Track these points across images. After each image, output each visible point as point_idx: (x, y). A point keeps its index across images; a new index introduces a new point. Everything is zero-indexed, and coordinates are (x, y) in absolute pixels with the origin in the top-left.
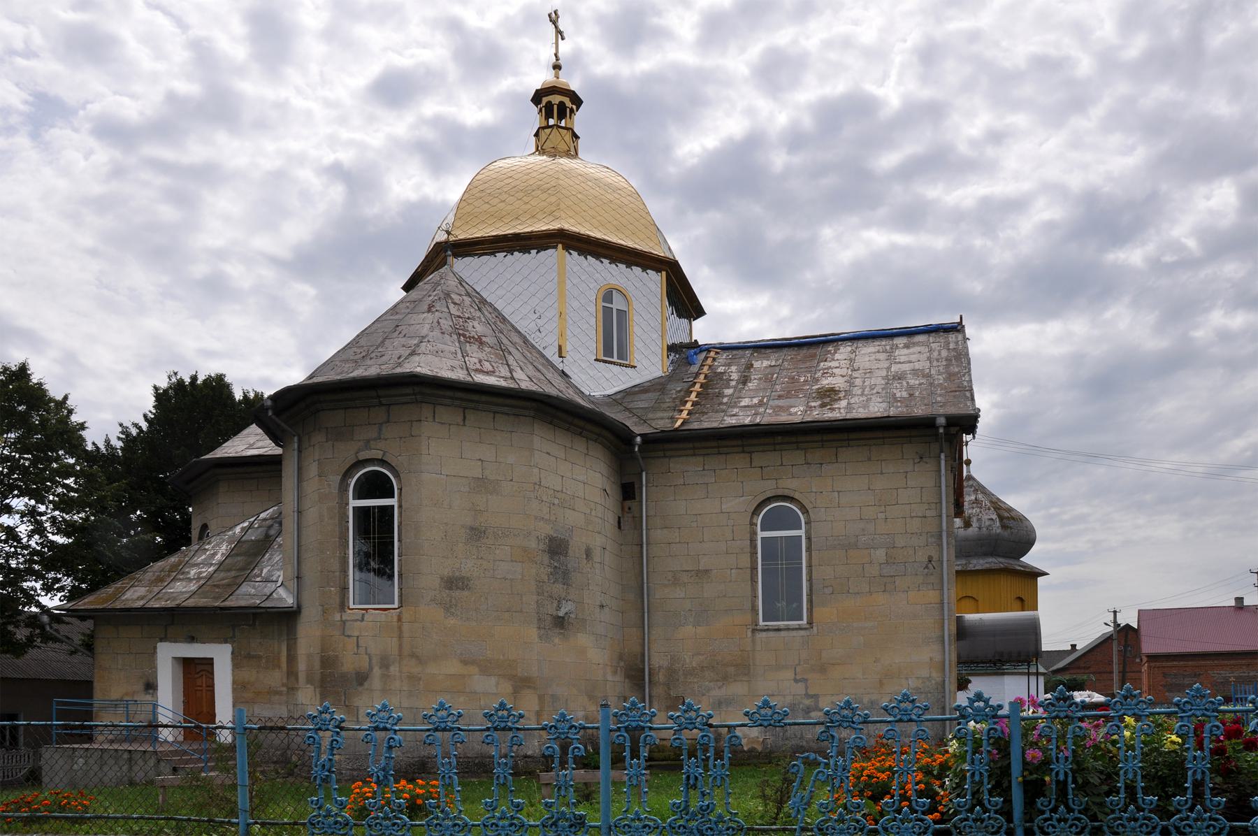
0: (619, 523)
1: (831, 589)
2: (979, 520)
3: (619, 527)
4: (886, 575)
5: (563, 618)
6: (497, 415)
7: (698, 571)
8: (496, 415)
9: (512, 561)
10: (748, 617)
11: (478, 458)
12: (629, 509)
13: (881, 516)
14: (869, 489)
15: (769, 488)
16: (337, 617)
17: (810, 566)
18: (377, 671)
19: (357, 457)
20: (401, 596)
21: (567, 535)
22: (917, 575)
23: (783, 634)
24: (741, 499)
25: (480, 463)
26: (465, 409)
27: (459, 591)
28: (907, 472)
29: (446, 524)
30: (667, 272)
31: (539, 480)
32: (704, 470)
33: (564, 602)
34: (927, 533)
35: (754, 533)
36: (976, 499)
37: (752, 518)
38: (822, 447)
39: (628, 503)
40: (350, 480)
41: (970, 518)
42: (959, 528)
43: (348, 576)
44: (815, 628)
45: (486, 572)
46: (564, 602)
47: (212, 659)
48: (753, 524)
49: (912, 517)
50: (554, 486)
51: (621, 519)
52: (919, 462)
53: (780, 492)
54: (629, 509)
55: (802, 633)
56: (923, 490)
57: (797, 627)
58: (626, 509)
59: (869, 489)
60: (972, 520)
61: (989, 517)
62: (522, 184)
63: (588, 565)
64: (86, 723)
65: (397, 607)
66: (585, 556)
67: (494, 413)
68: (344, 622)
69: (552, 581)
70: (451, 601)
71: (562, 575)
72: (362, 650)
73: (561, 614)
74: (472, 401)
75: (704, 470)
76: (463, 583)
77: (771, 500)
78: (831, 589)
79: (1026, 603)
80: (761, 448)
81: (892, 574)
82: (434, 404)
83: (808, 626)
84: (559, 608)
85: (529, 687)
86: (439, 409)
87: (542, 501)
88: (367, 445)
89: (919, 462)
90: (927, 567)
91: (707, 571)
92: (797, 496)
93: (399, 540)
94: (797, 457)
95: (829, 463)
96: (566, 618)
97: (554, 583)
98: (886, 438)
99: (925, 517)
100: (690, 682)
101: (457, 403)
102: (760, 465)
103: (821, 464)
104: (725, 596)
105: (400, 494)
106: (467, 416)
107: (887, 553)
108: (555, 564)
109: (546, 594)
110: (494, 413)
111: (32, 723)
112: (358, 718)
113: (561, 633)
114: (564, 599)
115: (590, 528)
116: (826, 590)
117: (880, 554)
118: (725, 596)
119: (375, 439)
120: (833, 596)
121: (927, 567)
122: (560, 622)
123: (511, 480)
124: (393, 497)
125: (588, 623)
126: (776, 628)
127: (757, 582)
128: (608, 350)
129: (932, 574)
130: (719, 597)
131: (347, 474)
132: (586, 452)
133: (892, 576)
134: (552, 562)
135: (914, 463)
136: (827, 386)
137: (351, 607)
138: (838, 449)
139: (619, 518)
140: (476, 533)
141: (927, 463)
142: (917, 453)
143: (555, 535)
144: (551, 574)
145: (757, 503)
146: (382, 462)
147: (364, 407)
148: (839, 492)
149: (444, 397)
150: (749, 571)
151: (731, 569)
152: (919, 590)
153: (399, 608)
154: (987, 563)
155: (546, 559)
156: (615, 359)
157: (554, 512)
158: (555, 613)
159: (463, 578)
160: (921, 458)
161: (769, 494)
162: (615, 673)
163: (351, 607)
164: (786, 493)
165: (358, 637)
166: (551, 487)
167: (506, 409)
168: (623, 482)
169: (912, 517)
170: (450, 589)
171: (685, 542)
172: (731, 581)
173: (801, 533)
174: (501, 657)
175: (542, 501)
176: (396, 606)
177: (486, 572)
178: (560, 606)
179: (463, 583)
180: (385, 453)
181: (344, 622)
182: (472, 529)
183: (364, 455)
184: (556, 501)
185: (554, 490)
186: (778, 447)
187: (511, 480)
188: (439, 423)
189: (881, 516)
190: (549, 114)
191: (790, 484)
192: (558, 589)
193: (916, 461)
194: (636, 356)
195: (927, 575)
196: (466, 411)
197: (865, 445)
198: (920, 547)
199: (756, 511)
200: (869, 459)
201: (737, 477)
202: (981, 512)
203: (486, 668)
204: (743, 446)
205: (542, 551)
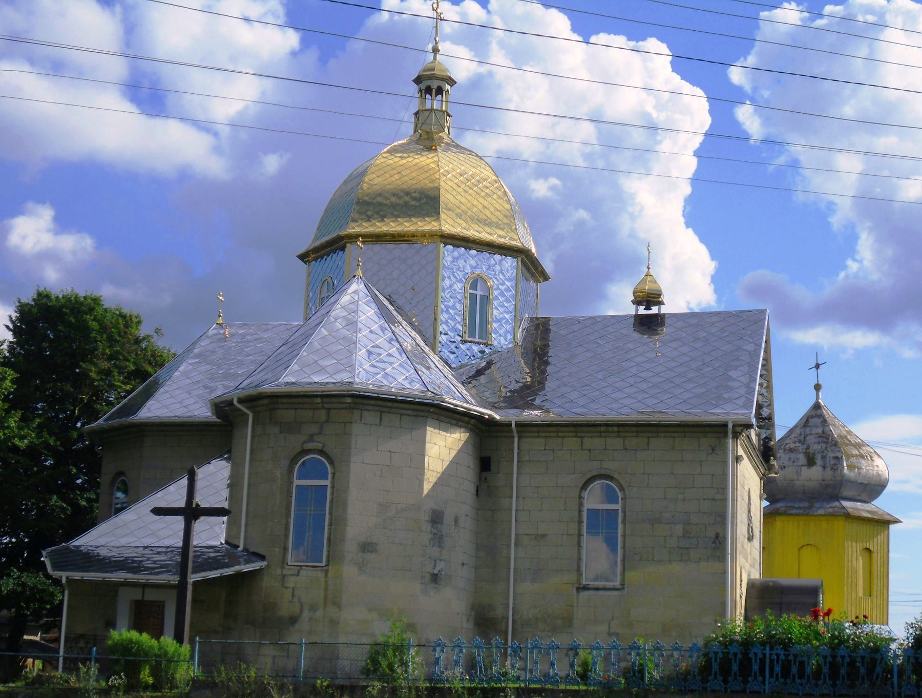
0: (477, 491)
2: (824, 457)
3: (477, 495)
4: (682, 547)
6: (403, 417)
9: (407, 530)
11: (388, 450)
14: (672, 473)
15: (594, 468)
16: (279, 571)
17: (624, 536)
18: (306, 614)
19: (303, 447)
20: (328, 556)
22: (706, 548)
23: (601, 593)
24: (575, 475)
26: (382, 412)
27: (369, 554)
32: (545, 449)
33: (438, 561)
36: (823, 432)
37: (580, 492)
39: (484, 474)
40: (295, 466)
41: (814, 454)
42: (802, 465)
43: (288, 539)
44: (626, 589)
47: (164, 602)
49: (704, 499)
50: (437, 469)
51: (479, 487)
52: (711, 454)
53: (603, 472)
54: (486, 479)
55: (616, 593)
57: (612, 587)
58: (483, 479)
59: (672, 473)
60: (816, 457)
61: (836, 455)
62: (410, 181)
64: (234, 641)
65: (324, 565)
66: (454, 524)
67: (401, 414)
68: (284, 576)
70: (363, 562)
71: (438, 539)
72: (296, 599)
73: (436, 572)
74: (386, 407)
75: (545, 449)
76: (372, 547)
77: (596, 477)
79: (874, 555)
80: (590, 435)
81: (687, 546)
82: (361, 409)
83: (620, 587)
86: (365, 413)
88: (311, 439)
89: (711, 454)
90: (714, 542)
92: (616, 476)
93: (330, 513)
95: (642, 450)
96: (439, 575)
97: (433, 547)
98: (687, 432)
100: (527, 631)
101: (377, 408)
102: (588, 448)
104: (557, 558)
105: (333, 477)
106: (383, 418)
107: (684, 528)
108: (435, 531)
110: (401, 414)
111: (228, 641)
112: (288, 653)
113: (435, 587)
116: (636, 556)
117: (679, 529)
118: (557, 558)
119: (318, 434)
121: (714, 542)
122: (435, 578)
124: (328, 480)
126: (596, 587)
131: (294, 461)
133: (687, 548)
135: (708, 454)
137: (289, 564)
138: (651, 439)
139: (478, 486)
141: (717, 454)
145: (584, 481)
146: (321, 452)
147: (310, 409)
148: (649, 474)
149: (367, 405)
150: (576, 537)
151: (563, 535)
153: (325, 566)
154: (831, 507)
158: (432, 572)
160: (713, 450)
161: (595, 473)
162: (468, 620)
163: (289, 564)
164: (608, 472)
165: (293, 588)
166: (435, 470)
167: (409, 412)
168: (482, 456)
169: (704, 499)
171: (528, 510)
173: (618, 507)
175: (429, 482)
176: (323, 564)
179: (372, 547)
180: (324, 445)
181: (284, 576)
183: (310, 446)
186: (603, 434)
188: (364, 424)
189: (680, 496)
192: (435, 551)
193: (710, 452)
196: (383, 414)
197: (671, 437)
198: (709, 524)
200: (673, 448)
201: (571, 458)
202: (826, 448)
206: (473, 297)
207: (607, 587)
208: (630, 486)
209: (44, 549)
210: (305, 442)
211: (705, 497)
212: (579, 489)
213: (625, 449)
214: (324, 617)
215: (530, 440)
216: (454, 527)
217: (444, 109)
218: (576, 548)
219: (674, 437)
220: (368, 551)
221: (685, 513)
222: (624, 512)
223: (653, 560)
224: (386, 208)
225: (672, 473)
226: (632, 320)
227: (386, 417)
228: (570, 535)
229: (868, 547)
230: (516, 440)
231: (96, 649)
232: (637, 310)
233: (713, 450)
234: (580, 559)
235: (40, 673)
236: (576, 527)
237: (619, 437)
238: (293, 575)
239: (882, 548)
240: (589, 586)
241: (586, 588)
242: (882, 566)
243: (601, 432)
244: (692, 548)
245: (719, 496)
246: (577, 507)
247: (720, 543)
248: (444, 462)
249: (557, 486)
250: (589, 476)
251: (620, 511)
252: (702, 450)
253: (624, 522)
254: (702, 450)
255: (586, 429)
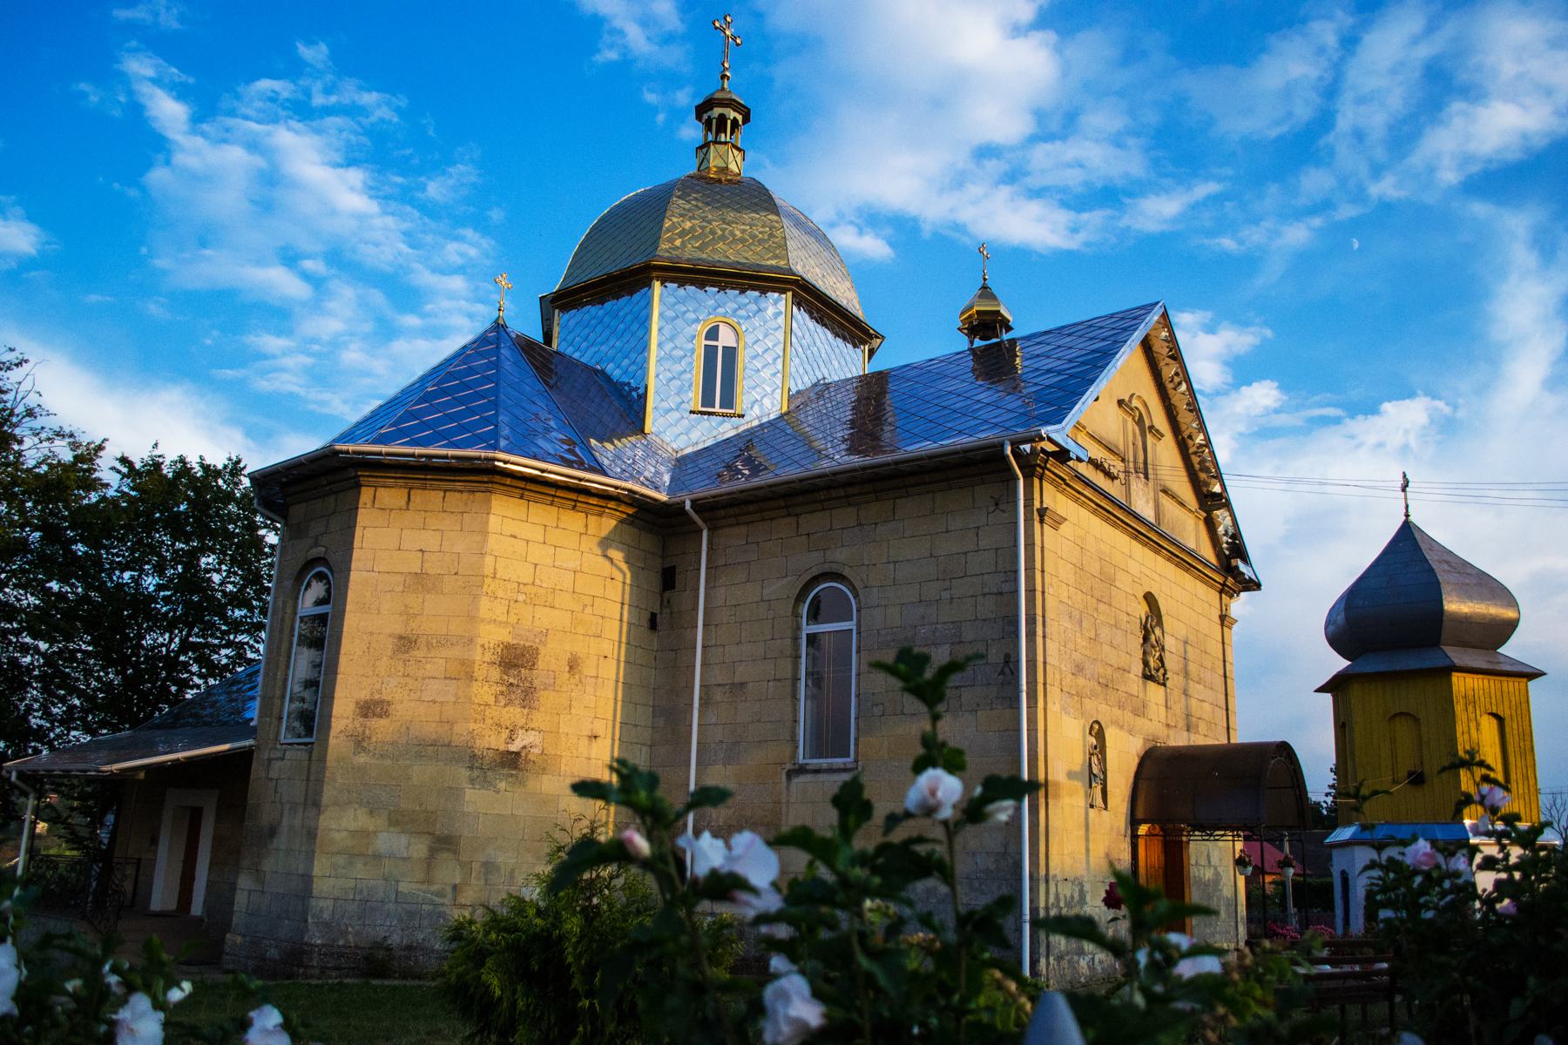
1: (881, 708)
3: (653, 624)
5: (518, 754)
7: (733, 684)
8: (448, 493)
9: (446, 678)
10: (788, 750)
12: (668, 601)
13: (946, 595)
15: (812, 562)
21: (537, 641)
24: (787, 579)
25: (420, 554)
27: (375, 719)
28: (978, 527)
29: (371, 634)
30: (793, 291)
31: (492, 571)
34: (1004, 618)
35: (798, 628)
38: (877, 500)
39: (667, 594)
45: (412, 694)
46: (520, 731)
47: (202, 808)
48: (797, 615)
49: (984, 595)
53: (827, 568)
54: (668, 601)
56: (999, 552)
57: (842, 766)
59: (931, 555)
63: (572, 680)
66: (567, 668)
69: (502, 704)
70: (364, 732)
73: (514, 748)
78: (881, 708)
84: (511, 739)
85: (449, 850)
86: (381, 492)
87: (496, 598)
91: (742, 684)
92: (847, 572)
94: (846, 516)
97: (506, 705)
99: (1001, 594)
103: (876, 524)
108: (511, 680)
109: (489, 722)
113: (512, 775)
114: (522, 728)
115: (581, 630)
120: (883, 719)
121: (1002, 673)
123: (456, 574)
125: (563, 760)
127: (799, 700)
128: (708, 399)
129: (1010, 683)
130: (753, 722)
132: (583, 530)
134: (506, 677)
136: (312, 407)
138: (897, 501)
140: (406, 643)
141: (1004, 511)
142: (992, 497)
143: (515, 642)
144: (502, 693)
148: (895, 562)
150: (788, 683)
152: (992, 709)
155: (495, 673)
156: (717, 409)
157: (516, 611)
159: (383, 702)
160: (997, 504)
161: (815, 571)
164: (835, 568)
166: (514, 578)
168: (666, 566)
169: (984, 595)
170: (366, 716)
172: (767, 699)
174: (418, 808)
177: (412, 694)
178: (514, 737)
182: (401, 638)
184: (521, 598)
185: (519, 583)
187: (456, 574)
189: (946, 595)
190: (708, 124)
191: (840, 556)
194: (742, 401)
195: (1002, 684)
198: (993, 640)
199: (800, 598)
200: (933, 512)
203: (398, 820)
204: (787, 507)
205: (489, 663)
206: (710, 352)
207: (835, 767)
208: (866, 587)
209: (1468, 839)
210: (311, 548)
211: (986, 590)
212: (793, 601)
213: (860, 525)
214: (303, 826)
215: (727, 530)
216: (567, 675)
217: (728, 140)
218: (788, 701)
219: (933, 492)
220: (374, 715)
221: (953, 623)
222: (859, 633)
223: (902, 713)
224: (150, 72)
225: (931, 555)
226: (969, 362)
227: (417, 496)
228: (779, 680)
229: (1494, 711)
230: (705, 534)
231: (1422, 883)
232: (972, 343)
233: (997, 504)
234: (795, 721)
235: (1428, 898)
236: (789, 667)
237: (850, 505)
238: (277, 759)
239: (1519, 712)
240: (808, 767)
241: (802, 770)
242: (1521, 737)
243: (821, 501)
244: (965, 686)
245: (1006, 588)
246: (789, 633)
247: (1012, 673)
248: (538, 567)
249: (762, 601)
250: (808, 577)
251: (854, 632)
252: (979, 508)
253: (858, 652)
254: (979, 508)
255: (800, 499)
